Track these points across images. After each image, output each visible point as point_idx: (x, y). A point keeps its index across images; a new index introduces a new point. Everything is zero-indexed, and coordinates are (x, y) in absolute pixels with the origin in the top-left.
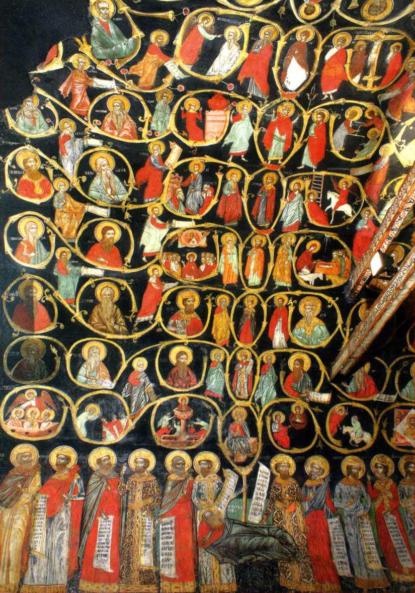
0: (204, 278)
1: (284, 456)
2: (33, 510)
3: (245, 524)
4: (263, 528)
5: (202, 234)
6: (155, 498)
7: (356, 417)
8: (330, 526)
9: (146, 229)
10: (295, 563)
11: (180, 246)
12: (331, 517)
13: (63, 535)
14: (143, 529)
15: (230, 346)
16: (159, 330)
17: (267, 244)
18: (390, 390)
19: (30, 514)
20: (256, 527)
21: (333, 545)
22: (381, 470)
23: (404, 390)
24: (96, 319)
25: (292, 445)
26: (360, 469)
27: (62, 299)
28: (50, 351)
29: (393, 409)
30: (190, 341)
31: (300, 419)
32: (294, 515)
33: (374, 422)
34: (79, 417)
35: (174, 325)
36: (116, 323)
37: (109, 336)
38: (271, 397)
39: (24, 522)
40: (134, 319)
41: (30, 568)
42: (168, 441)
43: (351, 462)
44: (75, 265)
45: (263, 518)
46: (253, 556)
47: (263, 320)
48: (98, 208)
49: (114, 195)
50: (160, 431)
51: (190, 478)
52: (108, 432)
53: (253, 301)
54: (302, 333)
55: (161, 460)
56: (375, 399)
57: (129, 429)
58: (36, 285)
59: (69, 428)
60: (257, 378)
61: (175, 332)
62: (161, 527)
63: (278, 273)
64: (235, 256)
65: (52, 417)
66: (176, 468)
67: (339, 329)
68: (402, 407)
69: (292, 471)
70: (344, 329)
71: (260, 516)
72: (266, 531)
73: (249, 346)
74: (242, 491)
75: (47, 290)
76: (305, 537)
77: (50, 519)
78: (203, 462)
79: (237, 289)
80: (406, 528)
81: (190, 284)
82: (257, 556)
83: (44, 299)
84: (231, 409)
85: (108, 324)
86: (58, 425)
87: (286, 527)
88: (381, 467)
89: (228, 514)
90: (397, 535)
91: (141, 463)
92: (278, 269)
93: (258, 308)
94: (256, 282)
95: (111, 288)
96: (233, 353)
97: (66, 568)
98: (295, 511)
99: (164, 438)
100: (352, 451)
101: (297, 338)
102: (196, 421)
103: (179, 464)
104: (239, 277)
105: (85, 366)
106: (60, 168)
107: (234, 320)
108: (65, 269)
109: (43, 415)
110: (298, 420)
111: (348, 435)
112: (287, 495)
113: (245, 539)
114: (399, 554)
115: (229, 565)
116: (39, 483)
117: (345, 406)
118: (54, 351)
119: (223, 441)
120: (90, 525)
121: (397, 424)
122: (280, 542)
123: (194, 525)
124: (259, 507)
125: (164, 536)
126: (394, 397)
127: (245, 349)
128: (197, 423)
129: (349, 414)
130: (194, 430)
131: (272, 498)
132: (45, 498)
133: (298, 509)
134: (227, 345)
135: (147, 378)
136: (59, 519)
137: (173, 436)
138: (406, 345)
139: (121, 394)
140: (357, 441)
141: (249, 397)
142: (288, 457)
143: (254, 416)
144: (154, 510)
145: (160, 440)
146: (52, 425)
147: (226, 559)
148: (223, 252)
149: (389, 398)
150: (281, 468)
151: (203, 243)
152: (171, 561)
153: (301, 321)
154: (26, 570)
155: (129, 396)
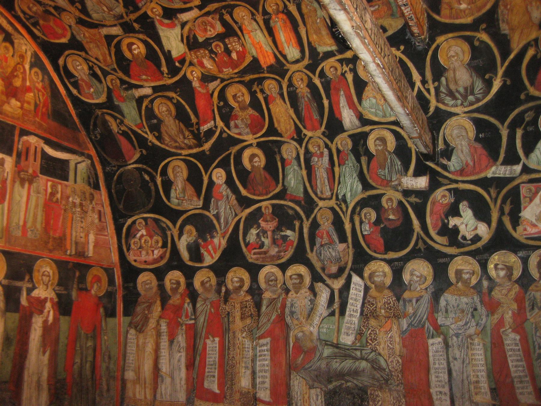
0: (242, 67)
1: (378, 263)
2: (159, 334)
3: (336, 346)
4: (356, 349)
5: (213, 18)
6: (252, 318)
7: (465, 203)
8: (430, 348)
9: (161, 34)
10: (387, 390)
11: (201, 40)
12: (433, 337)
13: (181, 357)
14: (243, 351)
15: (299, 139)
16: (224, 135)
17: (286, 6)
18: (512, 159)
19: (157, 338)
20: (348, 349)
21: (432, 371)
22: (502, 273)
23: (533, 156)
24: (167, 139)
25: (388, 248)
26: (473, 273)
27: (132, 125)
28: (144, 179)
29: (518, 186)
30: (258, 140)
31: (394, 215)
32: (389, 335)
33: (492, 206)
34: (181, 241)
35: (236, 126)
36: (184, 138)
37: (184, 152)
38: (356, 192)
39: (152, 345)
40: (198, 129)
41: (159, 387)
42: (259, 256)
43: (461, 265)
44: (126, 89)
45: (356, 339)
46: (343, 382)
47: (323, 99)
48: (110, 28)
49: (112, 11)
50: (249, 247)
51: (283, 296)
52: (205, 253)
53: (302, 79)
54: (373, 104)
55: (254, 278)
56: (490, 175)
57: (222, 248)
58: (108, 118)
59: (175, 252)
60: (336, 169)
61: (239, 134)
62: (258, 349)
63: (315, 36)
64: (259, 32)
65: (160, 244)
66: (269, 285)
67: (419, 88)
68: (531, 181)
69: (388, 281)
70: (426, 86)
71: (353, 336)
72: (358, 353)
73: (319, 133)
74: (335, 308)
75: (118, 121)
76: (400, 361)
77: (171, 342)
78: (294, 276)
79: (279, 69)
80: (532, 350)
81: (232, 78)
82: (347, 381)
83: (120, 129)
84: (315, 211)
85: (178, 140)
86: (167, 250)
87: (380, 349)
88: (502, 269)
89: (321, 334)
90: (518, 361)
91: (237, 282)
92: (313, 32)
93: (311, 85)
94: (296, 55)
95: (159, 109)
96: (304, 145)
97: (185, 387)
98: (390, 330)
99: (254, 254)
100: (462, 250)
101: (369, 111)
102: (282, 231)
103: (272, 281)
104: (275, 56)
105: (174, 187)
106: (55, 4)
107: (291, 107)
108: (121, 96)
109: (153, 242)
110: (391, 217)
111: (456, 230)
112: (383, 311)
113: (336, 362)
114: (517, 385)
115: (319, 390)
116: (159, 309)
117: (449, 190)
118: (147, 177)
119: (312, 250)
120: (200, 347)
121: (525, 208)
122: (373, 367)
123: (288, 347)
124: (353, 326)
125: (261, 358)
126: (518, 168)
127: (315, 136)
128: (283, 233)
129: (455, 200)
130: (281, 242)
131: (367, 315)
132: (166, 322)
133: (395, 328)
134: (296, 137)
135: (228, 190)
136: (178, 342)
137: (262, 250)
138: (525, 89)
139: (210, 212)
140: (469, 236)
141: (332, 194)
142: (383, 263)
143: (341, 218)
144: (252, 331)
145: (251, 257)
146: (162, 251)
147: (316, 384)
148: (245, 32)
149: (511, 170)
150: (376, 279)
151: (219, 28)
152: (266, 384)
153: (367, 89)
154: (157, 388)
155: (217, 213)
